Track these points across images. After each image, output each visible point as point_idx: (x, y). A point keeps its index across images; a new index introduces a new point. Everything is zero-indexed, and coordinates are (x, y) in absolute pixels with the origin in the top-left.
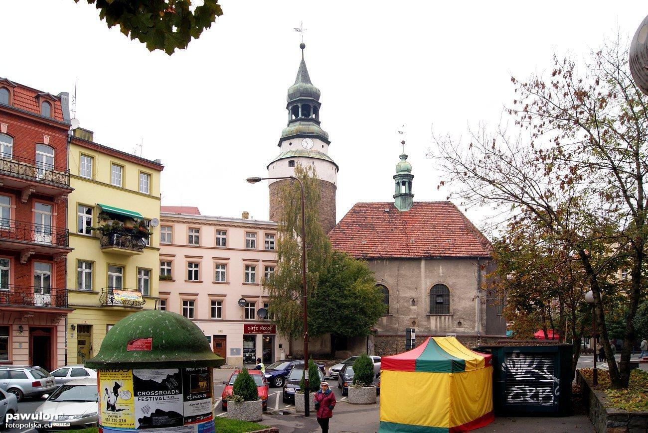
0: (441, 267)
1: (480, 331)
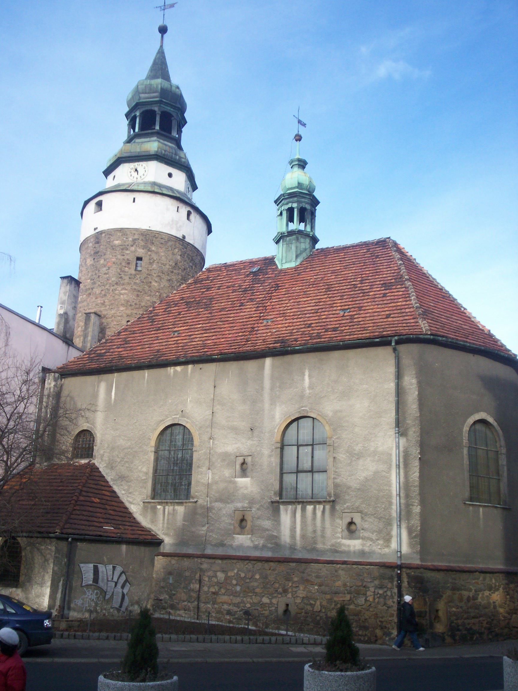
0: (307, 373)
1: (405, 549)
